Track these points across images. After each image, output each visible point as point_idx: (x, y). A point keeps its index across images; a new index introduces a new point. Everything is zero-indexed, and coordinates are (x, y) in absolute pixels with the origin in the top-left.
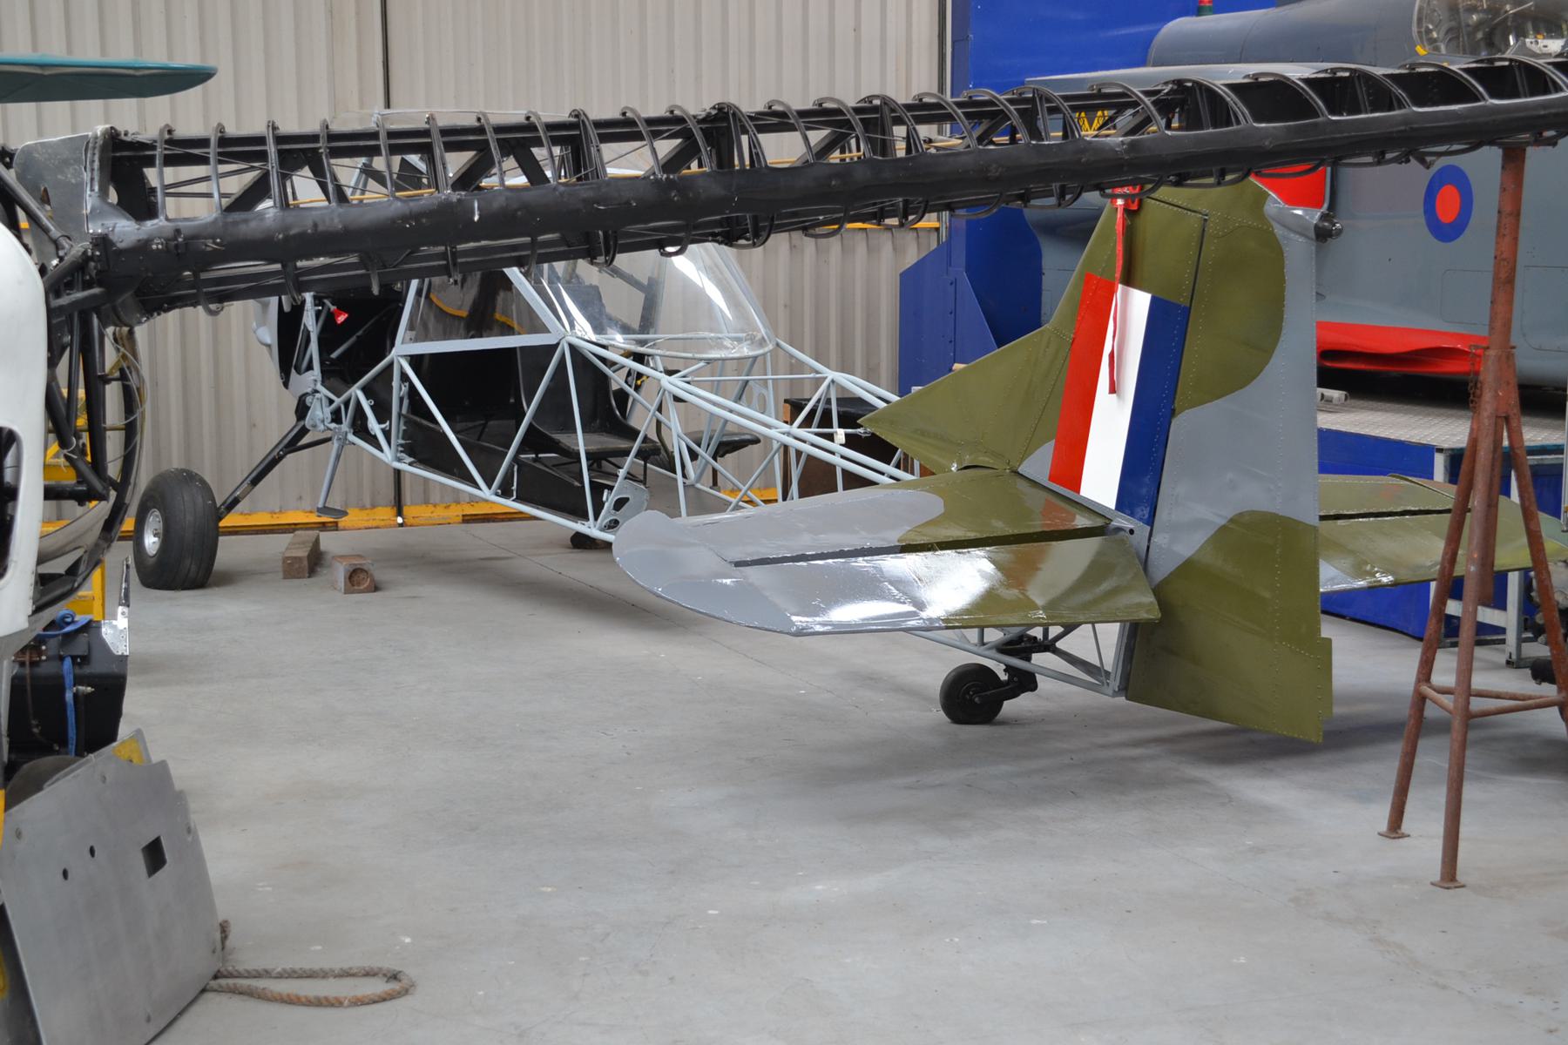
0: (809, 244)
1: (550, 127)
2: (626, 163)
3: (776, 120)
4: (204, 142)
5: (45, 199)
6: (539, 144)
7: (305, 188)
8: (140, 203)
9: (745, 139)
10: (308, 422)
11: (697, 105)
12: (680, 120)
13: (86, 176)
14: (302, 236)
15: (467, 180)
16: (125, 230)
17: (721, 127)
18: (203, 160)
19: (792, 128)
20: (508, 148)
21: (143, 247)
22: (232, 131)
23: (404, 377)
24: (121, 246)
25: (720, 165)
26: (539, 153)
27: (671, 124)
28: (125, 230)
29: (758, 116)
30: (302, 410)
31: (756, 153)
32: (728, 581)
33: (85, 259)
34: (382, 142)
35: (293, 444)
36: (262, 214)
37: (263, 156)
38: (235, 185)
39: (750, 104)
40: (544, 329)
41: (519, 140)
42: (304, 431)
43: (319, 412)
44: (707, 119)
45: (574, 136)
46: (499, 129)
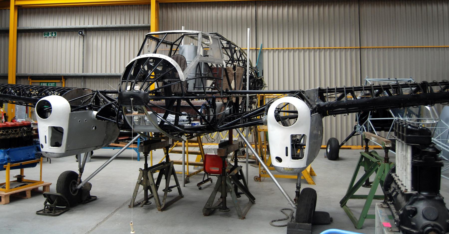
0: (419, 8)
1: (393, 85)
2: (406, 91)
3: (435, 84)
4: (334, 89)
5: (309, 98)
6: (391, 88)
7: (349, 96)
8: (323, 98)
9: (429, 87)
10: (356, 130)
11: (419, 82)
12: (416, 84)
13: (24, 120)
14: (350, 105)
15: (377, 95)
16: (322, 103)
17: (424, 85)
18: (334, 92)
19: (438, 85)
20: (385, 89)
21: (325, 106)
22: (329, 88)
23: (370, 124)
24: (321, 106)
25: (424, 92)
26: (390, 90)
27: (415, 85)
28: (322, 103)
29: (431, 83)
30: (355, 128)
31: (431, 90)
32: (415, 231)
33: (316, 108)
34: (363, 88)
35: (353, 134)
36: (343, 101)
37: (343, 91)
38: (339, 95)
39: (430, 81)
40: (392, 117)
41: (387, 88)
42: (355, 132)
43: (358, 129)
44: (422, 84)
45: (397, 87)
46: (383, 86)
